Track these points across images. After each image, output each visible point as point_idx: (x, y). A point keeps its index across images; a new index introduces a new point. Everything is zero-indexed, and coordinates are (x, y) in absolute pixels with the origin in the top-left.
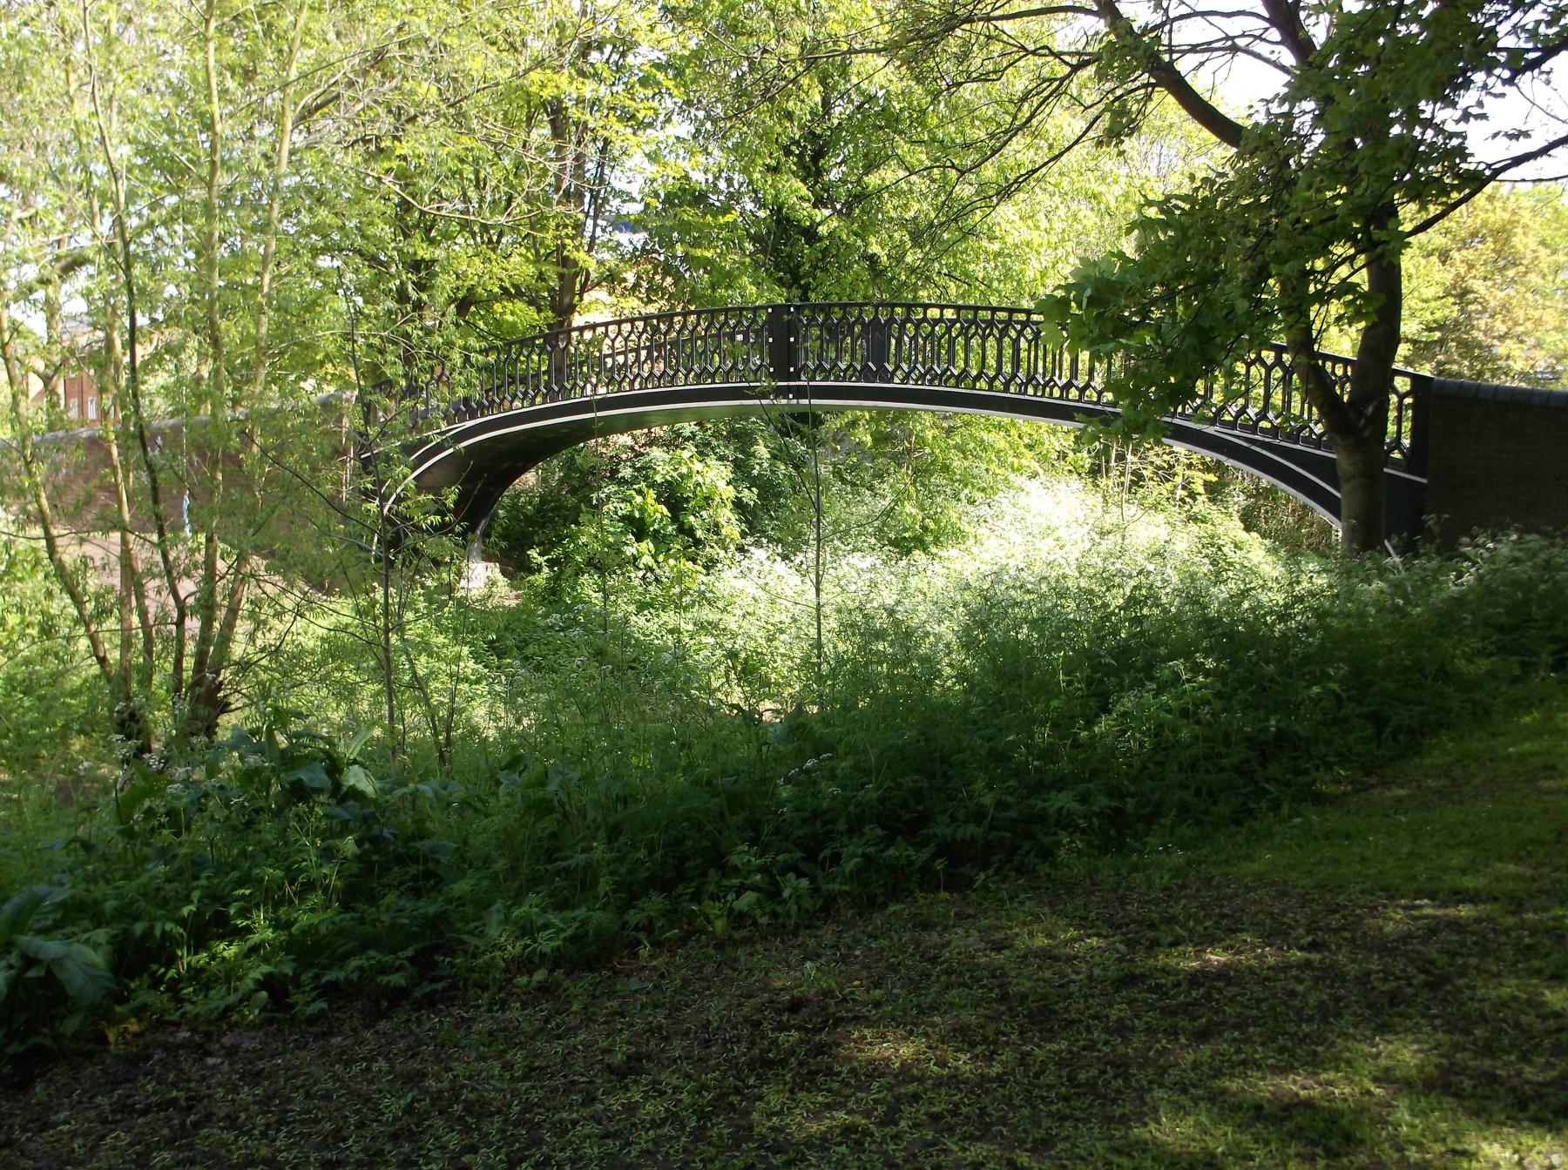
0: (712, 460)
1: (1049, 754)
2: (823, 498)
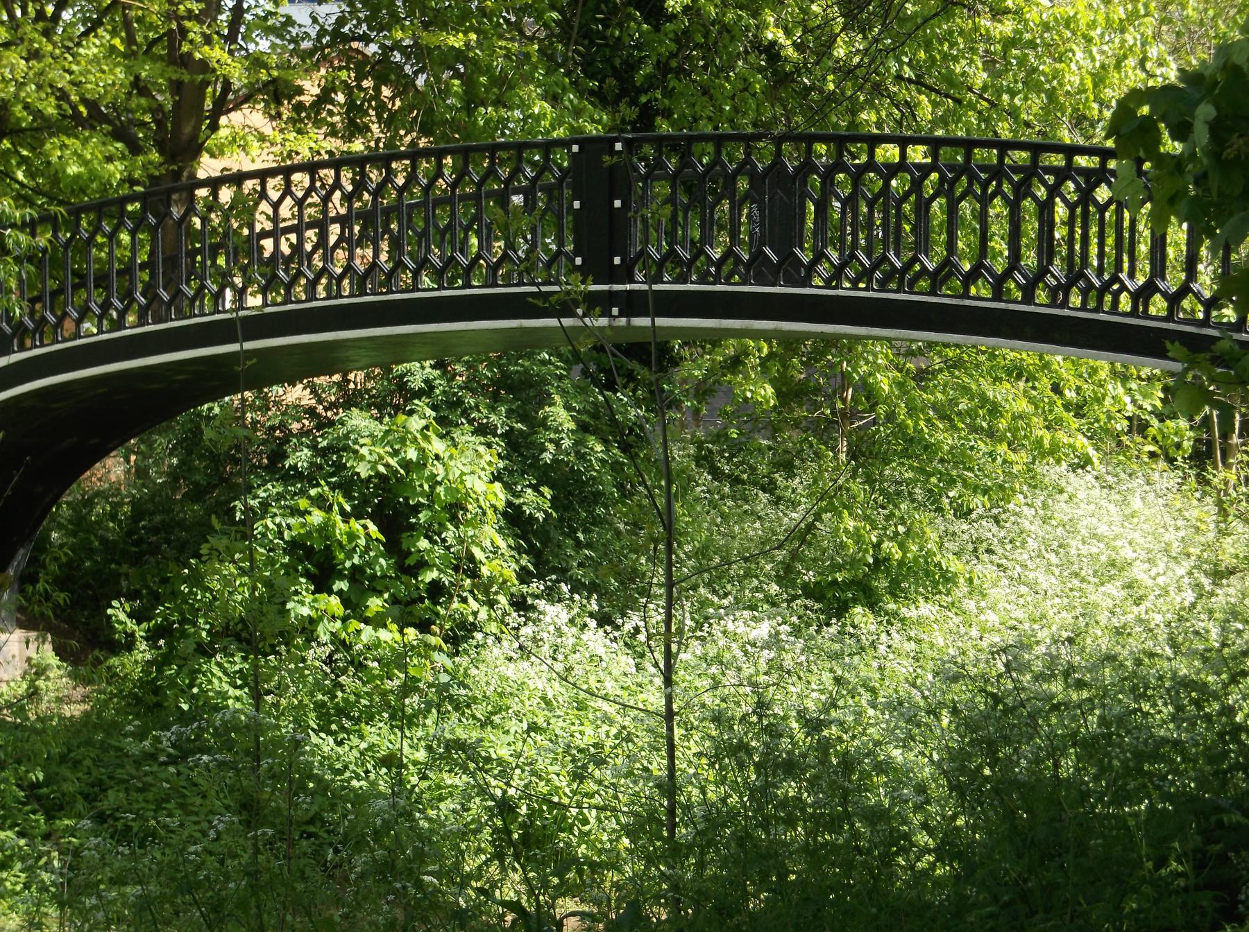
2: (678, 507)
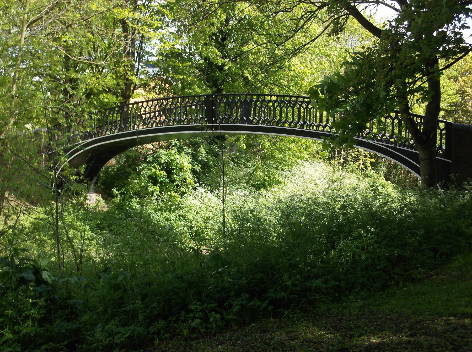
0: (183, 154)
1: (312, 265)
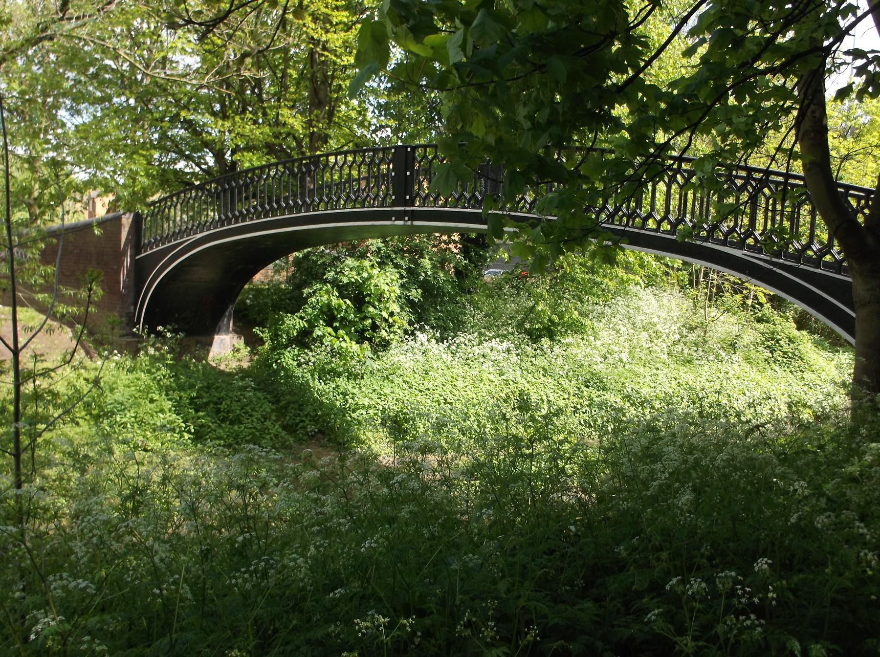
0: (390, 269)
